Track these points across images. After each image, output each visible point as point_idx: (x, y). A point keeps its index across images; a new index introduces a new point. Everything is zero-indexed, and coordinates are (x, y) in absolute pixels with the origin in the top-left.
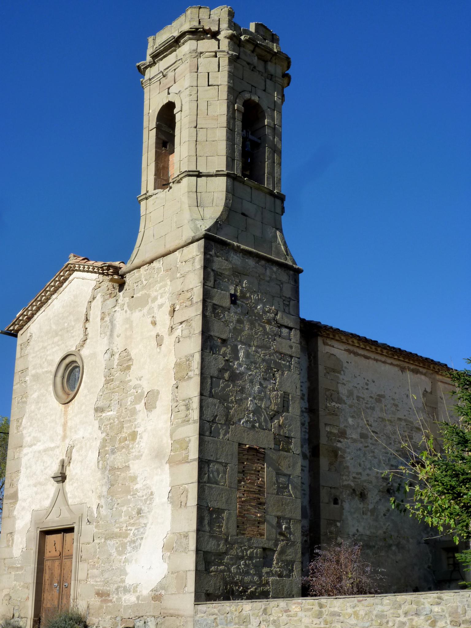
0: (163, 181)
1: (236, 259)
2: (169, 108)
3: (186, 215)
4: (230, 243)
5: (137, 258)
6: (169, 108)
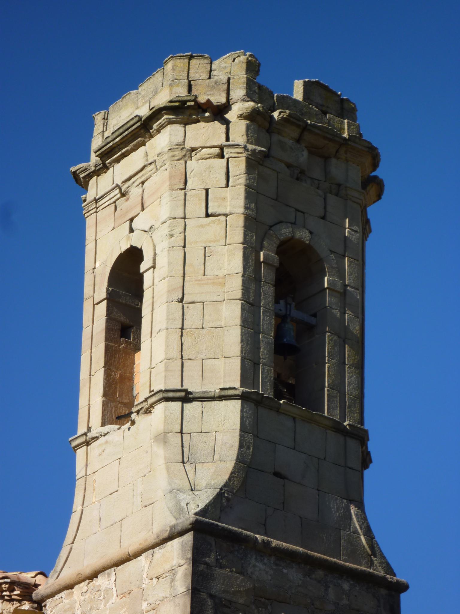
0: (120, 407)
1: (261, 570)
2: (131, 258)
3: (161, 481)
4: (248, 536)
5: (68, 567)
6: (131, 258)
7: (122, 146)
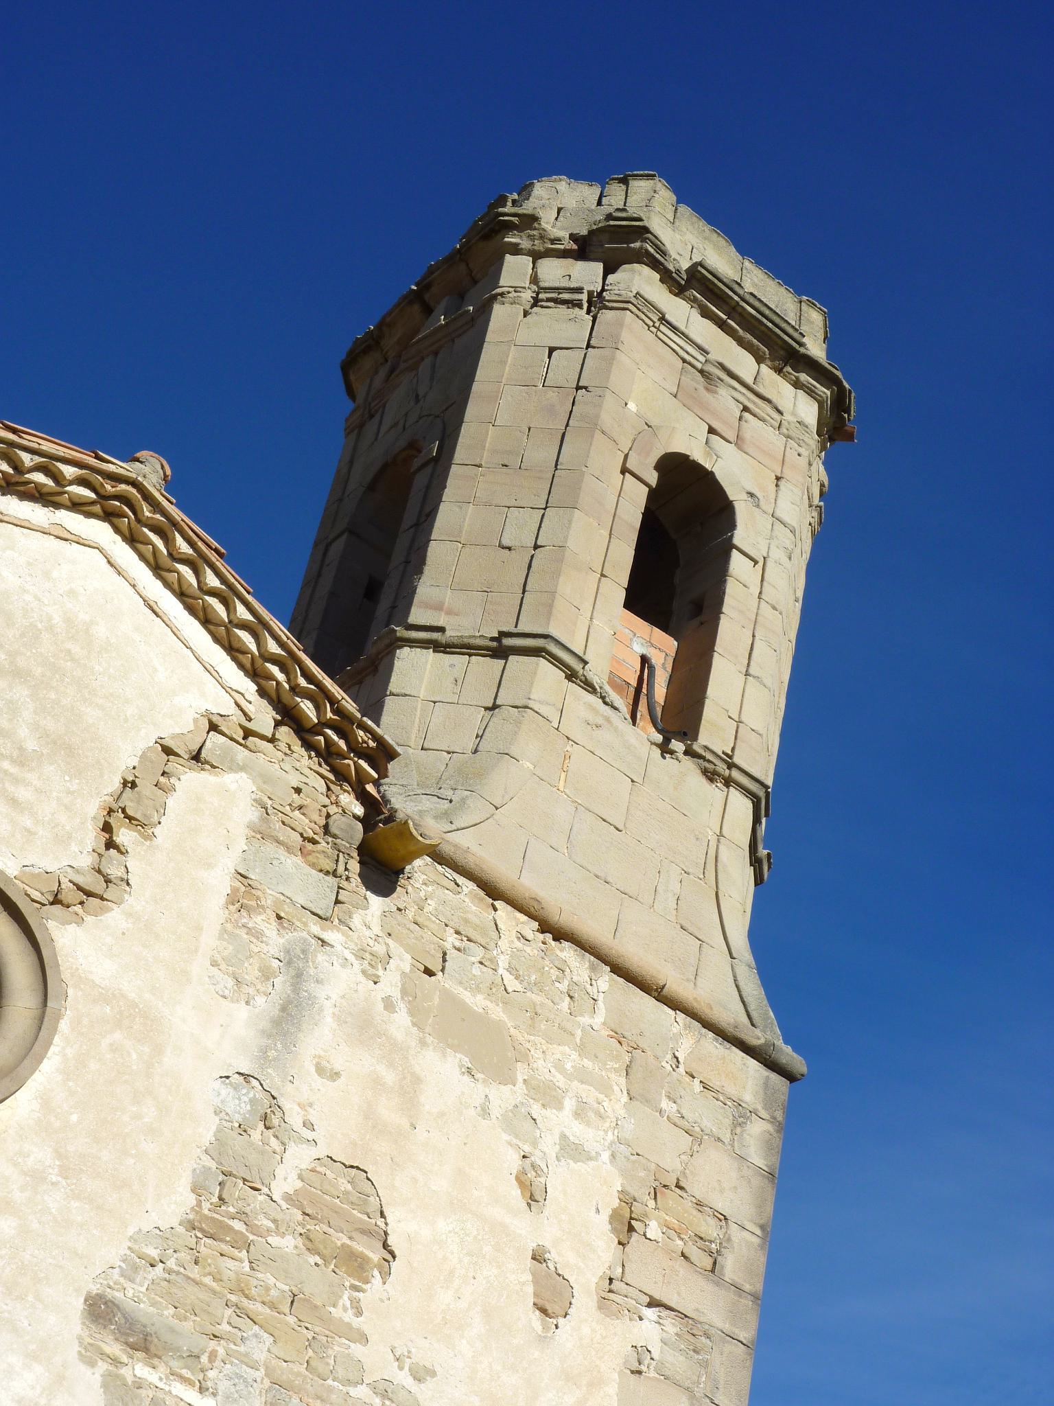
7: (737, 316)
